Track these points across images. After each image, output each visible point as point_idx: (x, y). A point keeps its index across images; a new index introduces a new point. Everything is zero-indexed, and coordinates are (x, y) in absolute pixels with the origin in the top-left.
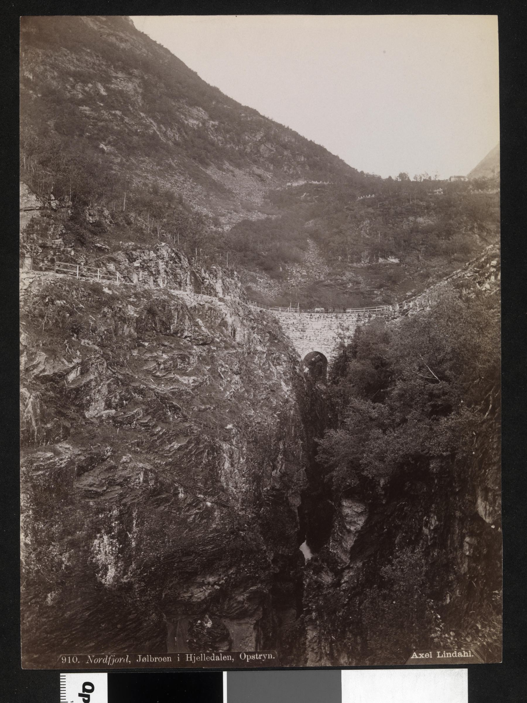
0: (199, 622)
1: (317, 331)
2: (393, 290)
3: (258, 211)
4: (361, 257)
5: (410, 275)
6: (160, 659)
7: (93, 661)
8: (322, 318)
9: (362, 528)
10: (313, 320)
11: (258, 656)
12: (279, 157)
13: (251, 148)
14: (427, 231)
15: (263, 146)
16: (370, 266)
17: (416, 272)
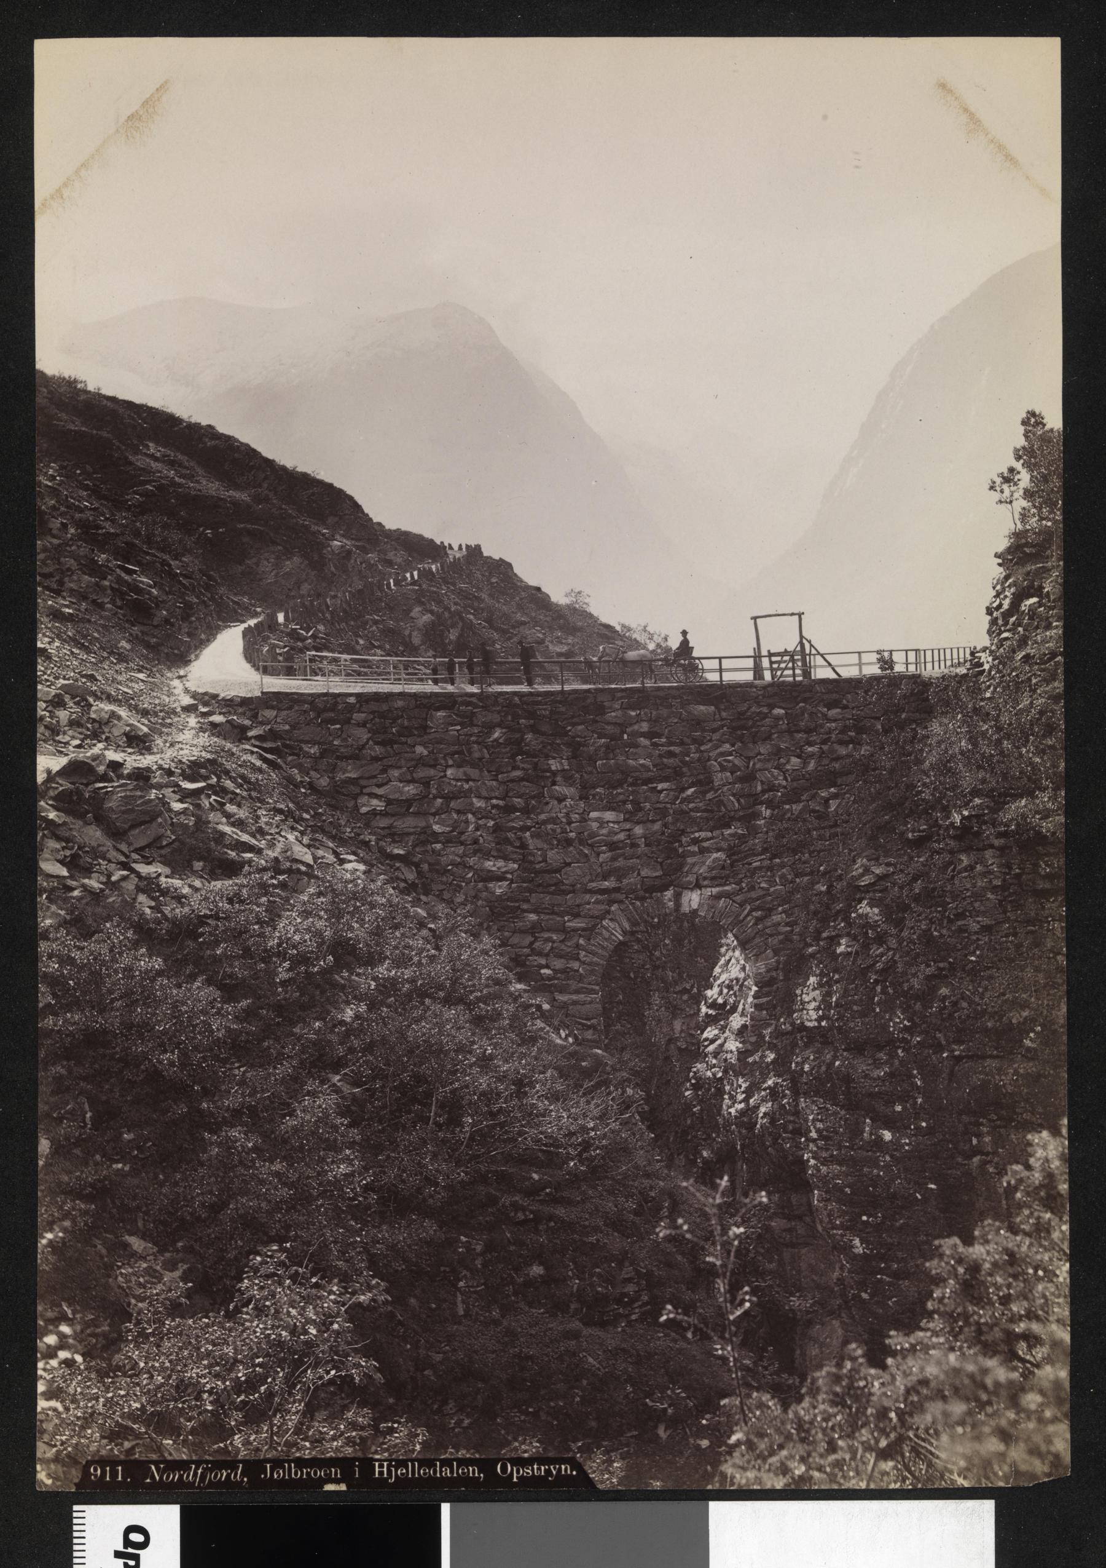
6: (315, 1474)
7: (161, 1478)
11: (539, 1469)
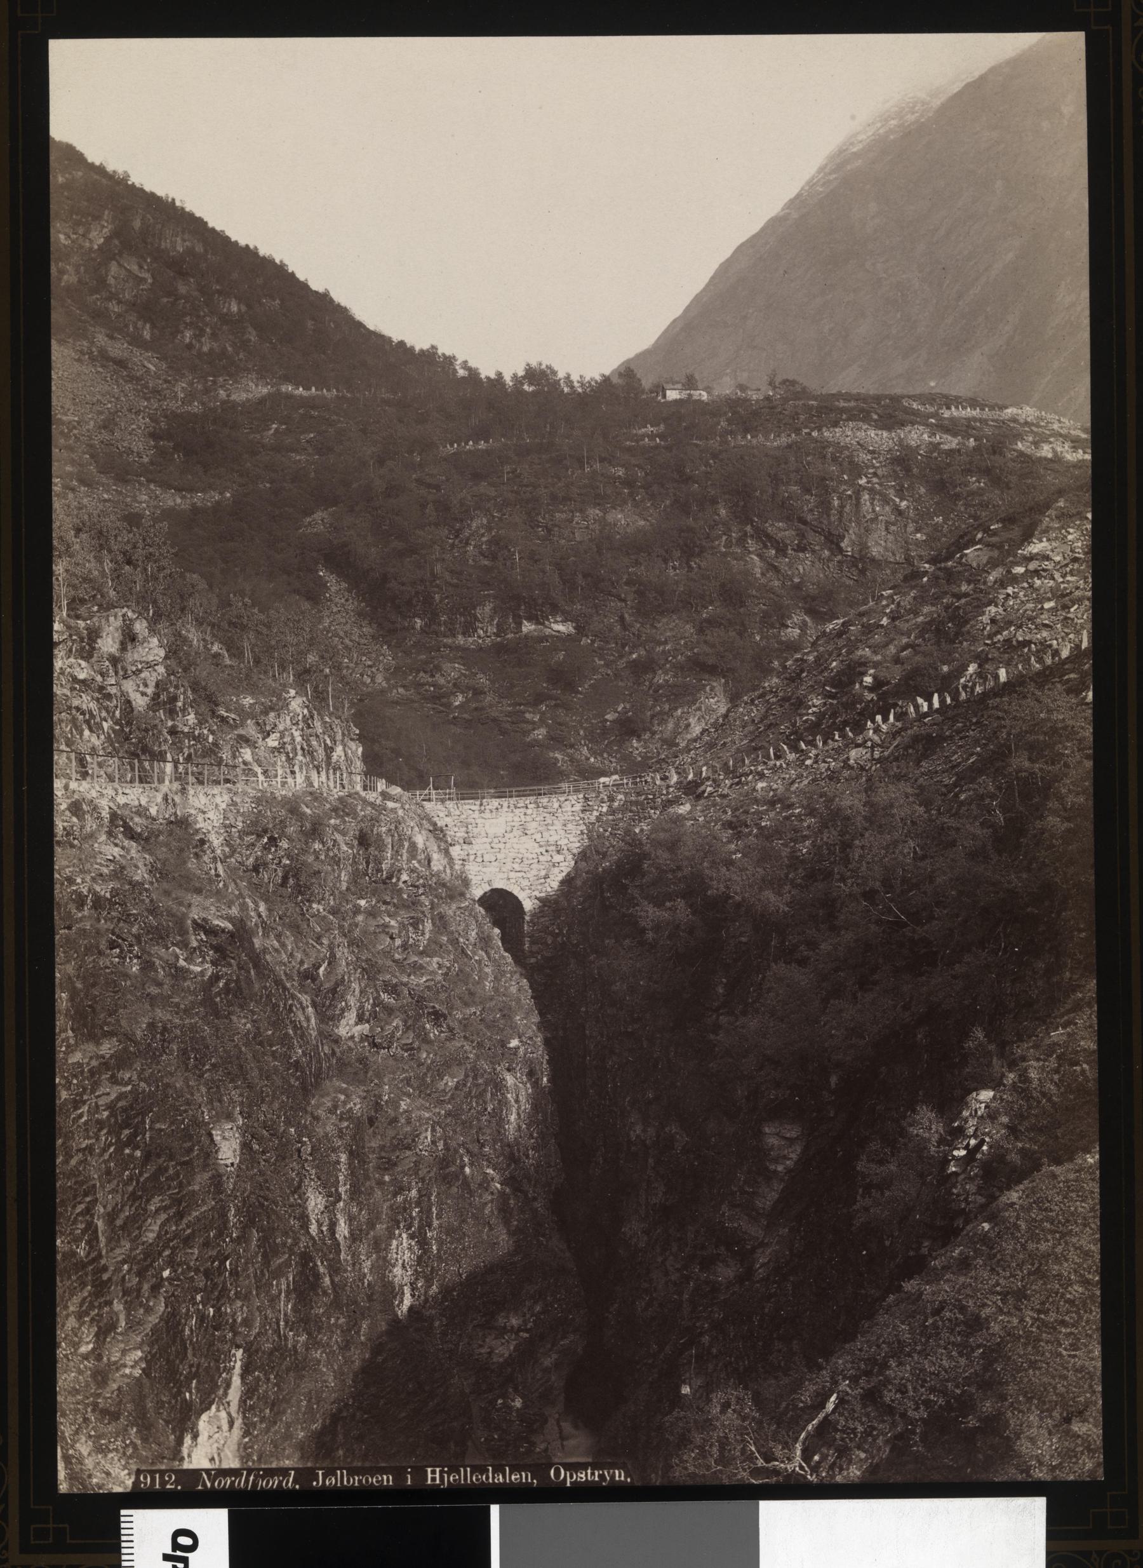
0: (500, 1401)
1: (496, 840)
2: (567, 707)
3: (149, 481)
4: (476, 619)
5: (607, 665)
8: (505, 809)
9: (796, 1163)
10: (487, 815)
12: (165, 300)
13: (77, 272)
14: (637, 546)
15: (114, 268)
16: (501, 643)
17: (621, 657)
